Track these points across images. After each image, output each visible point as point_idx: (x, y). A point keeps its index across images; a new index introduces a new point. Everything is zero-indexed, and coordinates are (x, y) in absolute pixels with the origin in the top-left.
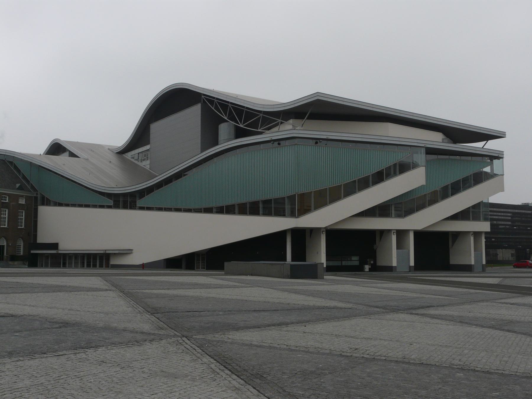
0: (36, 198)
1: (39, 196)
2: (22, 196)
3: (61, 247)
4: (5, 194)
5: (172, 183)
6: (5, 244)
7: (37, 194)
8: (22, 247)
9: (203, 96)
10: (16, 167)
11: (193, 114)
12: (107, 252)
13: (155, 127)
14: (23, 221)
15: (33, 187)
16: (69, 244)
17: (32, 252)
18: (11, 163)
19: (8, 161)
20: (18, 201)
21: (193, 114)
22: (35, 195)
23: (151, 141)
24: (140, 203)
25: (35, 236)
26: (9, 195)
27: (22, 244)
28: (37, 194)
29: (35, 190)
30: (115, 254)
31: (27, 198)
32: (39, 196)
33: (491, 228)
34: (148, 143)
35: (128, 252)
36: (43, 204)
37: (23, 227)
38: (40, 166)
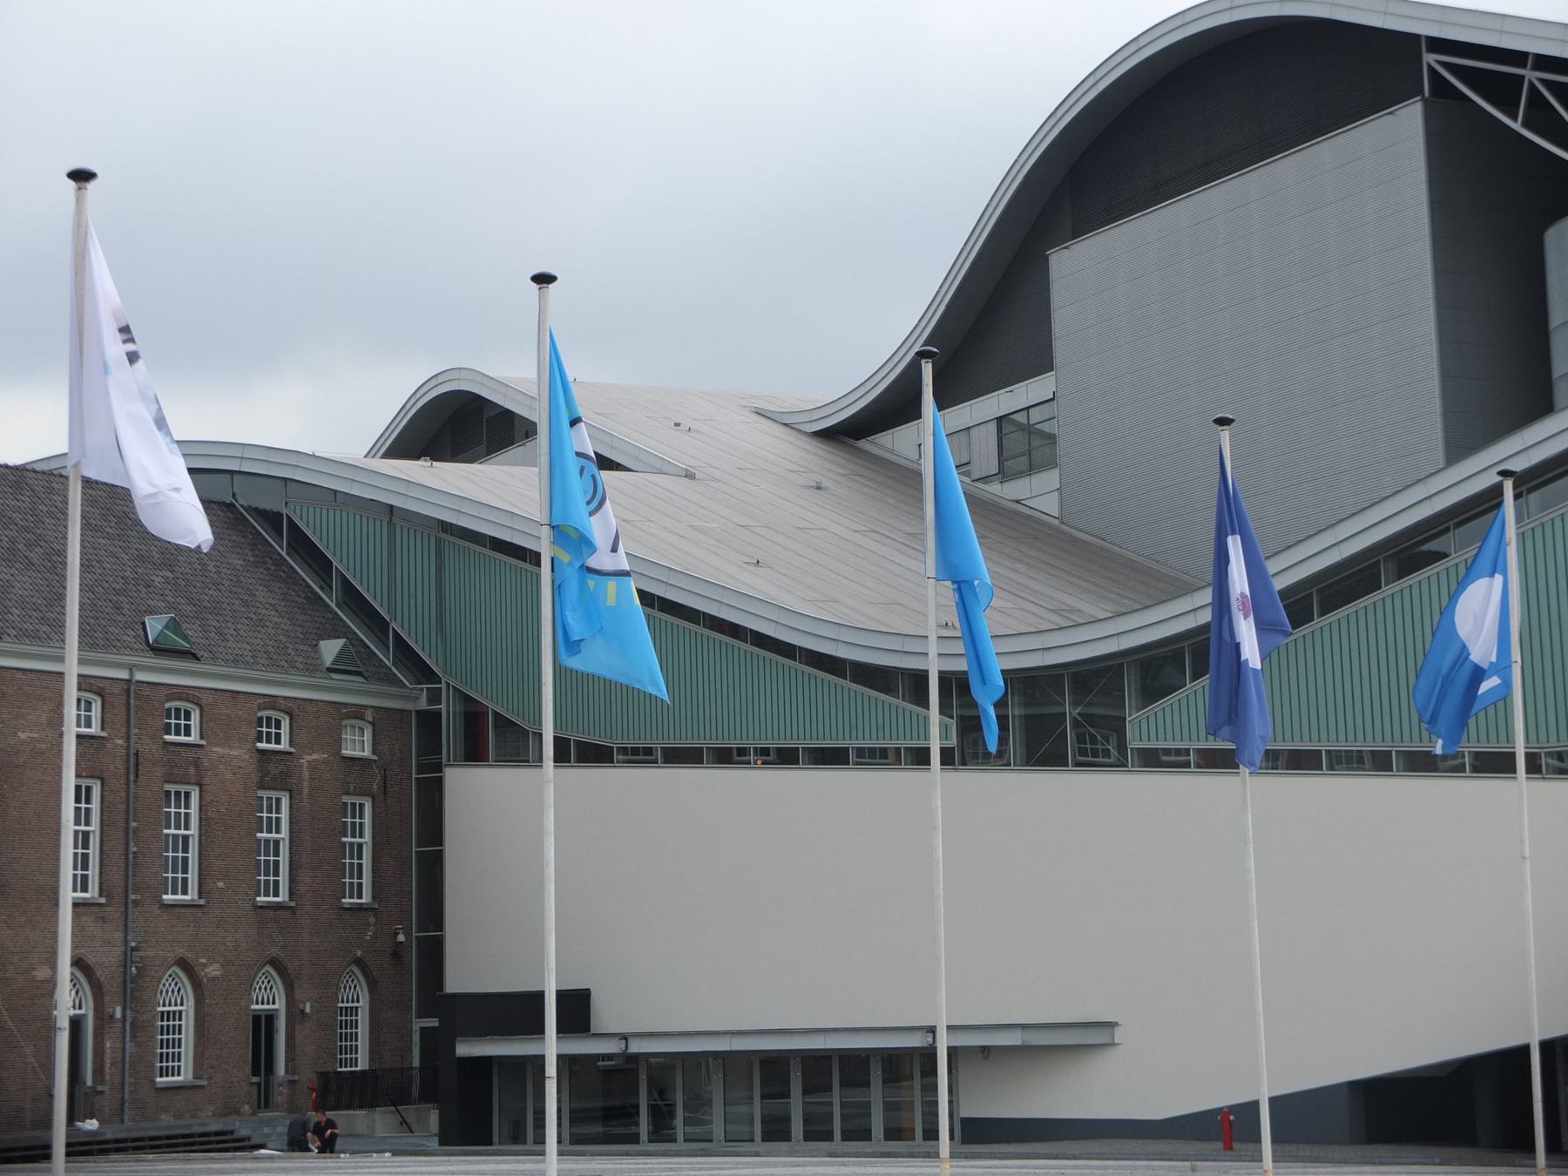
0: (429, 722)
1: (448, 708)
2: (357, 713)
3: (608, 1015)
4: (272, 702)
5: (1375, 597)
6: (280, 1005)
7: (435, 697)
8: (363, 1019)
9: (1430, 58)
10: (301, 544)
11: (1382, 163)
12: (636, 1047)
13: (1086, 273)
14: (366, 861)
15: (405, 653)
16: (665, 1000)
17: (465, 1049)
18: (273, 520)
19: (249, 509)
20: (338, 742)
21: (1382, 163)
22: (423, 704)
23: (1057, 362)
24: (1145, 725)
25: (433, 954)
26: (293, 709)
27: (363, 1004)
28: (435, 697)
29: (424, 673)
30: (985, 1050)
31: (385, 723)
32: (448, 708)
33: (454, 996)
34: (1041, 362)
35: (1086, 1039)
36: (474, 754)
37: (366, 899)
38: (446, 527)
